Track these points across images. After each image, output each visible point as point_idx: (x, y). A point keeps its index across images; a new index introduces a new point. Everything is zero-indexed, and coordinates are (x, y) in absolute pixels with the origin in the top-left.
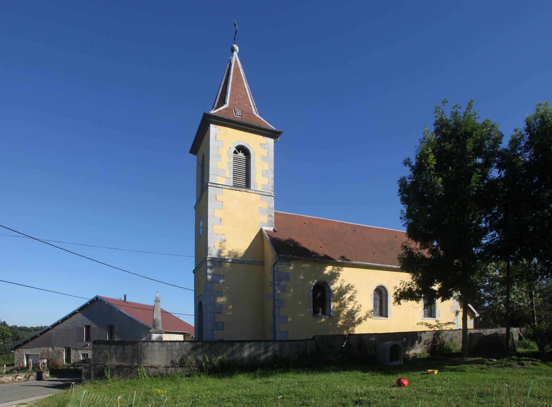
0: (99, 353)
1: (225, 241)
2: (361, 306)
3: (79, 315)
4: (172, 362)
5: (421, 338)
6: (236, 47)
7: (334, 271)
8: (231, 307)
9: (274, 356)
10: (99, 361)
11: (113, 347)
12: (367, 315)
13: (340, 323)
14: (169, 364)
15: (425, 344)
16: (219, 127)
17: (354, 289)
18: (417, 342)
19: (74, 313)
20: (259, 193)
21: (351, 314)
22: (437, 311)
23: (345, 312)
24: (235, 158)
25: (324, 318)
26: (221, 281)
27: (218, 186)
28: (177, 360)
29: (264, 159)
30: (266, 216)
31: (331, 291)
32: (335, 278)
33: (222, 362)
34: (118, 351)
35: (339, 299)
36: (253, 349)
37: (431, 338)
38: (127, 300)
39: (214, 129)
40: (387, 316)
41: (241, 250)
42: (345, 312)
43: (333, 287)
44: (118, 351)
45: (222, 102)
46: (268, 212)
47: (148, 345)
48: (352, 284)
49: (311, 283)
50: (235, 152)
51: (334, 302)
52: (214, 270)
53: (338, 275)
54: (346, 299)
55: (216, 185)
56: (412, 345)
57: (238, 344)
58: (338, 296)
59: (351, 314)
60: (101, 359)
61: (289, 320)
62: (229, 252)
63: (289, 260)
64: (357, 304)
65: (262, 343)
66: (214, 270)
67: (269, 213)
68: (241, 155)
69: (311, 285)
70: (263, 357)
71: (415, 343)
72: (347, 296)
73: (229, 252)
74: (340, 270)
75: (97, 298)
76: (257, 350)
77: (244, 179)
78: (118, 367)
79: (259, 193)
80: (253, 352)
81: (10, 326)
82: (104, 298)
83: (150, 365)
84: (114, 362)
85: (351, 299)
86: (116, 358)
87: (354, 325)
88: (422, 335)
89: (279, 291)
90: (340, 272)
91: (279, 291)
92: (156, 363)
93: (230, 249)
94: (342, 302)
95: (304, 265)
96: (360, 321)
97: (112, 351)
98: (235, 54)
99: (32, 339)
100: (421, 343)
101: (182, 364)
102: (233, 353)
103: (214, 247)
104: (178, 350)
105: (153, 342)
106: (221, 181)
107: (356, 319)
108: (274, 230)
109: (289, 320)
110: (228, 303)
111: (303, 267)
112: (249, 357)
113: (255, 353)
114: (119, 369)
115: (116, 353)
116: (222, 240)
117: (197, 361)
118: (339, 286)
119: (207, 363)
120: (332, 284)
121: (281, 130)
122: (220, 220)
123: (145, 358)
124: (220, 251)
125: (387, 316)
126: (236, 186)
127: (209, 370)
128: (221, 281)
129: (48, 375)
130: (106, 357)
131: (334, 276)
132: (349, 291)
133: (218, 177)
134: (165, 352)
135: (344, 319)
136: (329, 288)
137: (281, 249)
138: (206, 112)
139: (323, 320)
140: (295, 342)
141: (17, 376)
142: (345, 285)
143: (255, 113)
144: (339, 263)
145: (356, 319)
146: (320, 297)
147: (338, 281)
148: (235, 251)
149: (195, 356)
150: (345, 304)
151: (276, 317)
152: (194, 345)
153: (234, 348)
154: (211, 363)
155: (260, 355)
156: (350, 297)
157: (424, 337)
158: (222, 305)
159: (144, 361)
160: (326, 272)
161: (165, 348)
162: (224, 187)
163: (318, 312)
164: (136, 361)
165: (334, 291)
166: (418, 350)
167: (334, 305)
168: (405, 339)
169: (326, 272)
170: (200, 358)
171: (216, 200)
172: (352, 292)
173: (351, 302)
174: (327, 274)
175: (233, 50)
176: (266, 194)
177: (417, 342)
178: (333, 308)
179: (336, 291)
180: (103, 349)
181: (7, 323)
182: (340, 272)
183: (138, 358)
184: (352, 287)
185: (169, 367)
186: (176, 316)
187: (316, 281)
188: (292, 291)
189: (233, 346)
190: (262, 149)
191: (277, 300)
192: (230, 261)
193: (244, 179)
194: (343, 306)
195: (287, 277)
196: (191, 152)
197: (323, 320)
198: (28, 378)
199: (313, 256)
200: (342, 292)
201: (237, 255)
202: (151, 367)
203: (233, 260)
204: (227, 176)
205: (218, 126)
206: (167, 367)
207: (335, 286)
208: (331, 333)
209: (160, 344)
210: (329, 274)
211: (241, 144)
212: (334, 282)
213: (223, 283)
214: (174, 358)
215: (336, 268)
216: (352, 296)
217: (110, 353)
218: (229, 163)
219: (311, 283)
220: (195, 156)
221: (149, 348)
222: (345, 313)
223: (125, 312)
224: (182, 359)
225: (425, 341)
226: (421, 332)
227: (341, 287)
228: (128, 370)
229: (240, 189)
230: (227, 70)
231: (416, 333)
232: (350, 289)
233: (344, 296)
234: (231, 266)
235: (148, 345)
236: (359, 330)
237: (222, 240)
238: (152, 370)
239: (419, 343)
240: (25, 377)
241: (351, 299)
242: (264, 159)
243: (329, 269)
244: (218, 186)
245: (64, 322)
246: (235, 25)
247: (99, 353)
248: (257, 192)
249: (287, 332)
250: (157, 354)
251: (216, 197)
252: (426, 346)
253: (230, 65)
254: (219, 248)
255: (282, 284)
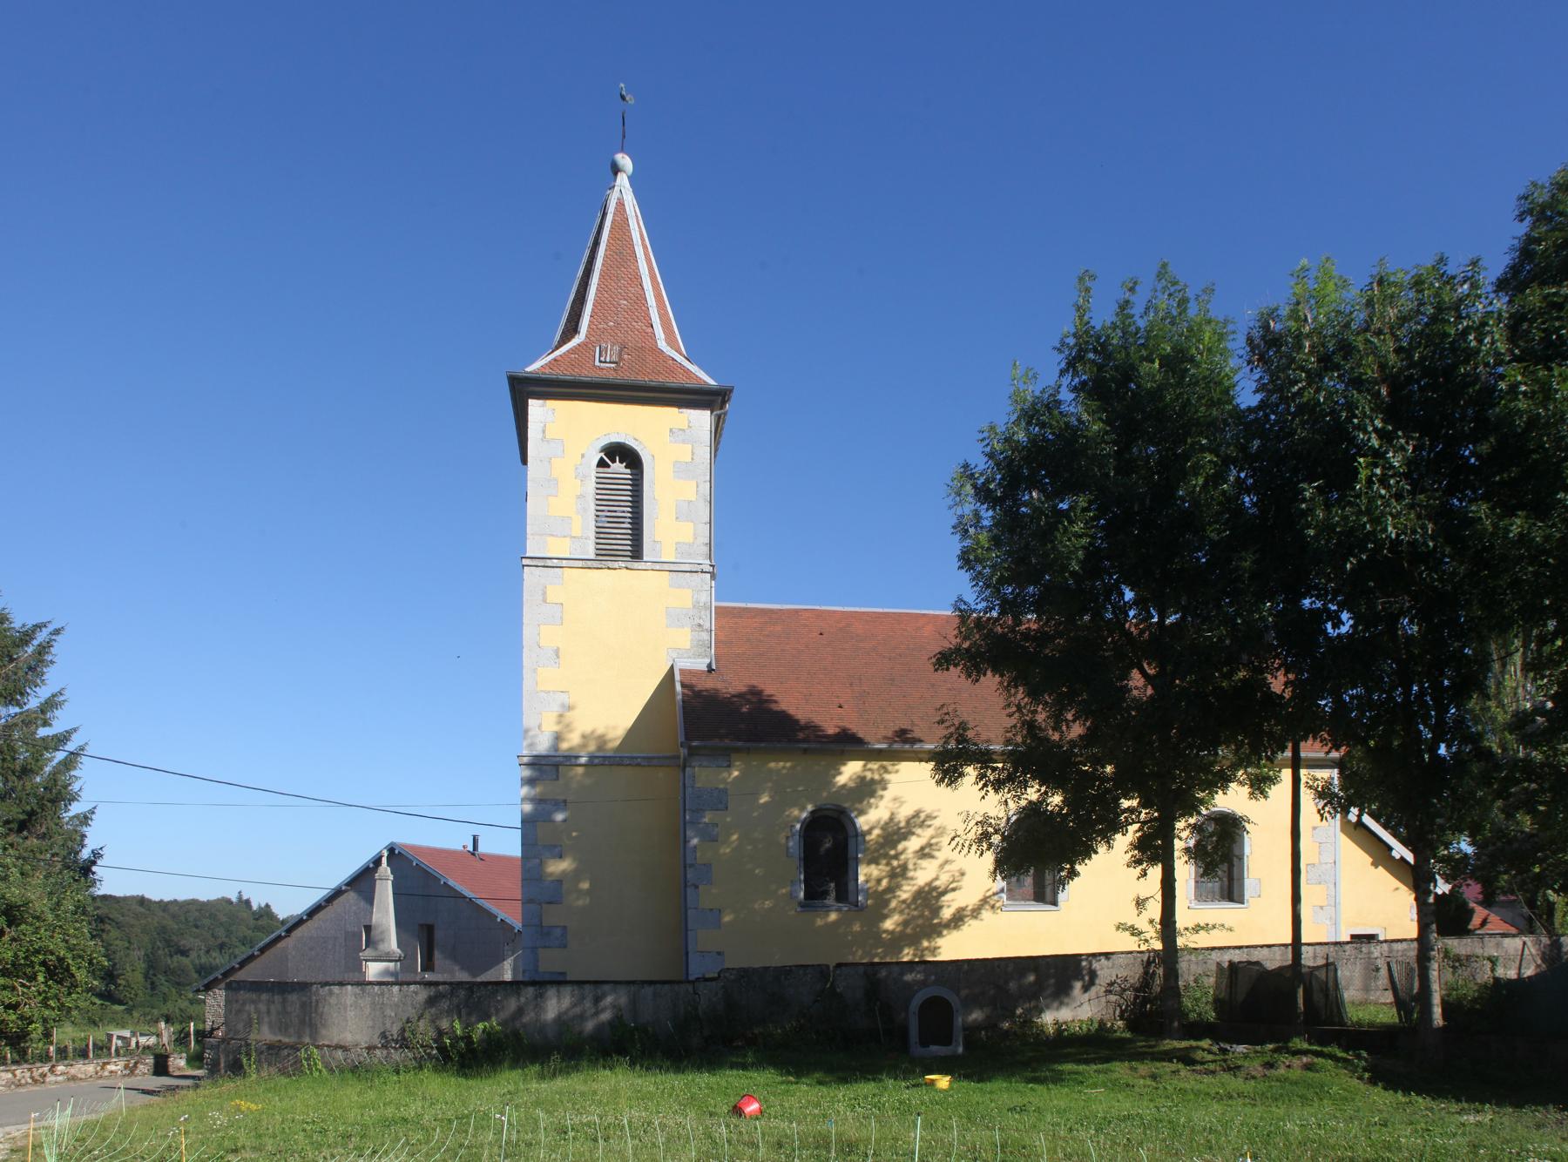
0: (239, 1011)
1: (570, 708)
2: (963, 874)
3: (351, 896)
4: (383, 1035)
5: (1093, 975)
6: (625, 161)
7: (869, 775)
8: (585, 885)
9: (617, 1023)
10: (237, 1032)
11: (264, 997)
12: (985, 901)
13: (889, 924)
14: (377, 1042)
15: (1108, 992)
16: (551, 404)
17: (936, 823)
18: (1078, 985)
19: (337, 893)
20: (666, 567)
21: (929, 897)
22: (1247, 882)
23: (906, 893)
24: (600, 481)
25: (839, 910)
26: (559, 817)
27: (549, 563)
28: (395, 1031)
29: (682, 470)
30: (687, 630)
31: (860, 835)
32: (872, 794)
33: (489, 1034)
34: (272, 1007)
35: (886, 856)
36: (566, 1002)
37: (1134, 974)
38: (482, 849)
41: (614, 728)
42: (906, 893)
43: (863, 822)
44: (272, 1007)
45: (572, 329)
47: (331, 993)
48: (928, 809)
49: (796, 812)
50: (602, 464)
51: (869, 863)
52: (538, 789)
53: (883, 784)
54: (909, 854)
55: (543, 562)
56: (1061, 992)
57: (531, 990)
58: (882, 846)
59: (929, 897)
60: (240, 1026)
61: (727, 918)
62: (584, 736)
63: (724, 756)
64: (947, 867)
65: (587, 987)
66: (538, 789)
67: (697, 621)
68: (618, 467)
69: (797, 819)
70: (590, 1026)
71: (1071, 988)
72: (913, 844)
73: (584, 736)
74: (887, 771)
76: (574, 1005)
77: (624, 535)
78: (270, 1047)
79: (666, 567)
80: (568, 1010)
81: (281, 917)
82: (413, 847)
83: (335, 1042)
84: (265, 1034)
85: (925, 853)
86: (270, 1023)
87: (935, 930)
88: (1095, 965)
89: (695, 841)
90: (887, 776)
91: (695, 841)
92: (348, 1038)
93: (588, 729)
94: (895, 863)
95: (772, 765)
96: (958, 920)
97: (262, 1007)
98: (623, 180)
100: (1094, 990)
101: (404, 1043)
102: (520, 1011)
103: (540, 727)
104: (397, 1005)
105: (371, 983)
106: (557, 547)
107: (947, 914)
108: (709, 665)
109: (727, 918)
110: (577, 875)
111: (770, 770)
112: (560, 1020)
113: (571, 1014)
114: (273, 1050)
115: (268, 1012)
116: (563, 706)
117: (441, 1033)
118: (885, 816)
119: (455, 1039)
120: (862, 812)
121: (727, 384)
122: (557, 652)
123: (324, 1026)
124: (558, 738)
125: (1055, 903)
126: (605, 554)
127: (462, 1056)
128: (559, 817)
129: (182, 1063)
130: (249, 1024)
131: (867, 789)
132: (919, 831)
133: (550, 539)
134: (368, 1011)
135: (901, 912)
136: (854, 824)
137: (711, 722)
138: (518, 370)
139: (833, 916)
140: (667, 987)
141: (105, 1064)
142: (903, 813)
143: (662, 344)
144: (880, 751)
145: (947, 914)
146: (828, 850)
147: (882, 804)
148: (600, 731)
149: (433, 1021)
150: (904, 868)
152: (432, 991)
153: (523, 1000)
154: (468, 1039)
155: (582, 1017)
156: (922, 849)
157: (1105, 972)
158: (559, 881)
159: (324, 1032)
160: (842, 779)
161: (368, 999)
162: (564, 563)
163: (824, 895)
164: (308, 1031)
165: (869, 832)
166: (1078, 1011)
167: (867, 873)
168: (1032, 978)
169: (842, 779)
170: (445, 1024)
171: (545, 601)
172: (928, 833)
173: (924, 863)
174: (844, 786)
175: (616, 169)
176: (687, 568)
177: (1078, 985)
178: (867, 881)
179: (876, 832)
180: (244, 1004)
181: (275, 909)
182: (887, 776)
183: (311, 1025)
184: (929, 817)
185: (375, 1048)
187: (810, 808)
188: (735, 837)
189: (519, 995)
190: (673, 441)
192: (583, 760)
193: (624, 535)
194: (899, 874)
195: (719, 800)
197: (833, 916)
198: (131, 1070)
199: (801, 735)
200: (895, 834)
201: (605, 742)
202: (338, 1047)
203: (592, 757)
204: (577, 531)
206: (370, 1048)
207: (871, 819)
208: (859, 956)
209: (357, 990)
210: (852, 784)
212: (870, 806)
213: (565, 821)
214: (388, 1025)
215: (874, 765)
216: (930, 845)
217: (258, 1011)
218: (581, 497)
219: (796, 812)
221: (333, 1000)
222: (904, 896)
223: (459, 887)
224: (403, 1030)
225: (1111, 984)
226: (1094, 955)
227: (891, 819)
228: (284, 1058)
229: (610, 564)
230: (594, 230)
231: (1075, 959)
232: (922, 825)
233: (900, 847)
234: (586, 774)
235: (331, 993)
236: (952, 947)
237: (563, 706)
238: (339, 1054)
239: (1086, 989)
240: (126, 1067)
241: (925, 853)
242: (682, 470)
243: (851, 770)
244: (549, 563)
245: (316, 917)
246: (623, 98)
247: (239, 1011)
248: (660, 566)
249: (719, 953)
250: (351, 1014)
251: (544, 593)
252: (1113, 998)
253: (604, 215)
254: (556, 728)
255: (706, 820)
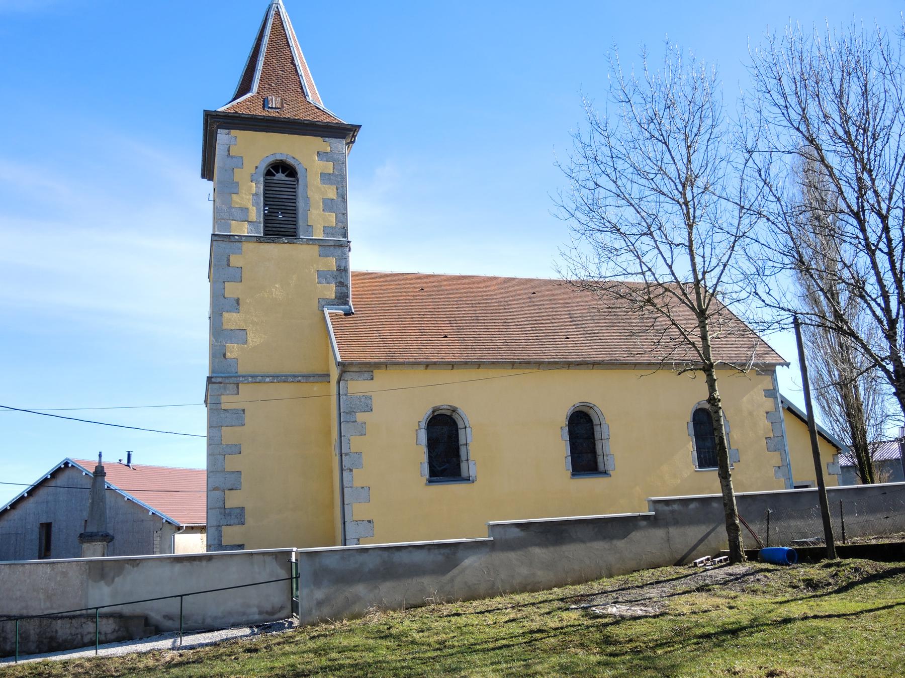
24: (267, 185)
39: (223, 137)
40: (430, 481)
46: (335, 277)
68: (280, 176)
75: (65, 466)
82: (83, 462)
99: (830, 616)
122: (238, 301)
125: (430, 481)
151: (346, 490)
171: (228, 265)
186: (128, 495)
191: (346, 454)
196: (203, 176)
205: (233, 132)
211: (279, 157)
218: (256, 194)
220: (211, 183)
249: (369, 521)
251: (228, 260)
